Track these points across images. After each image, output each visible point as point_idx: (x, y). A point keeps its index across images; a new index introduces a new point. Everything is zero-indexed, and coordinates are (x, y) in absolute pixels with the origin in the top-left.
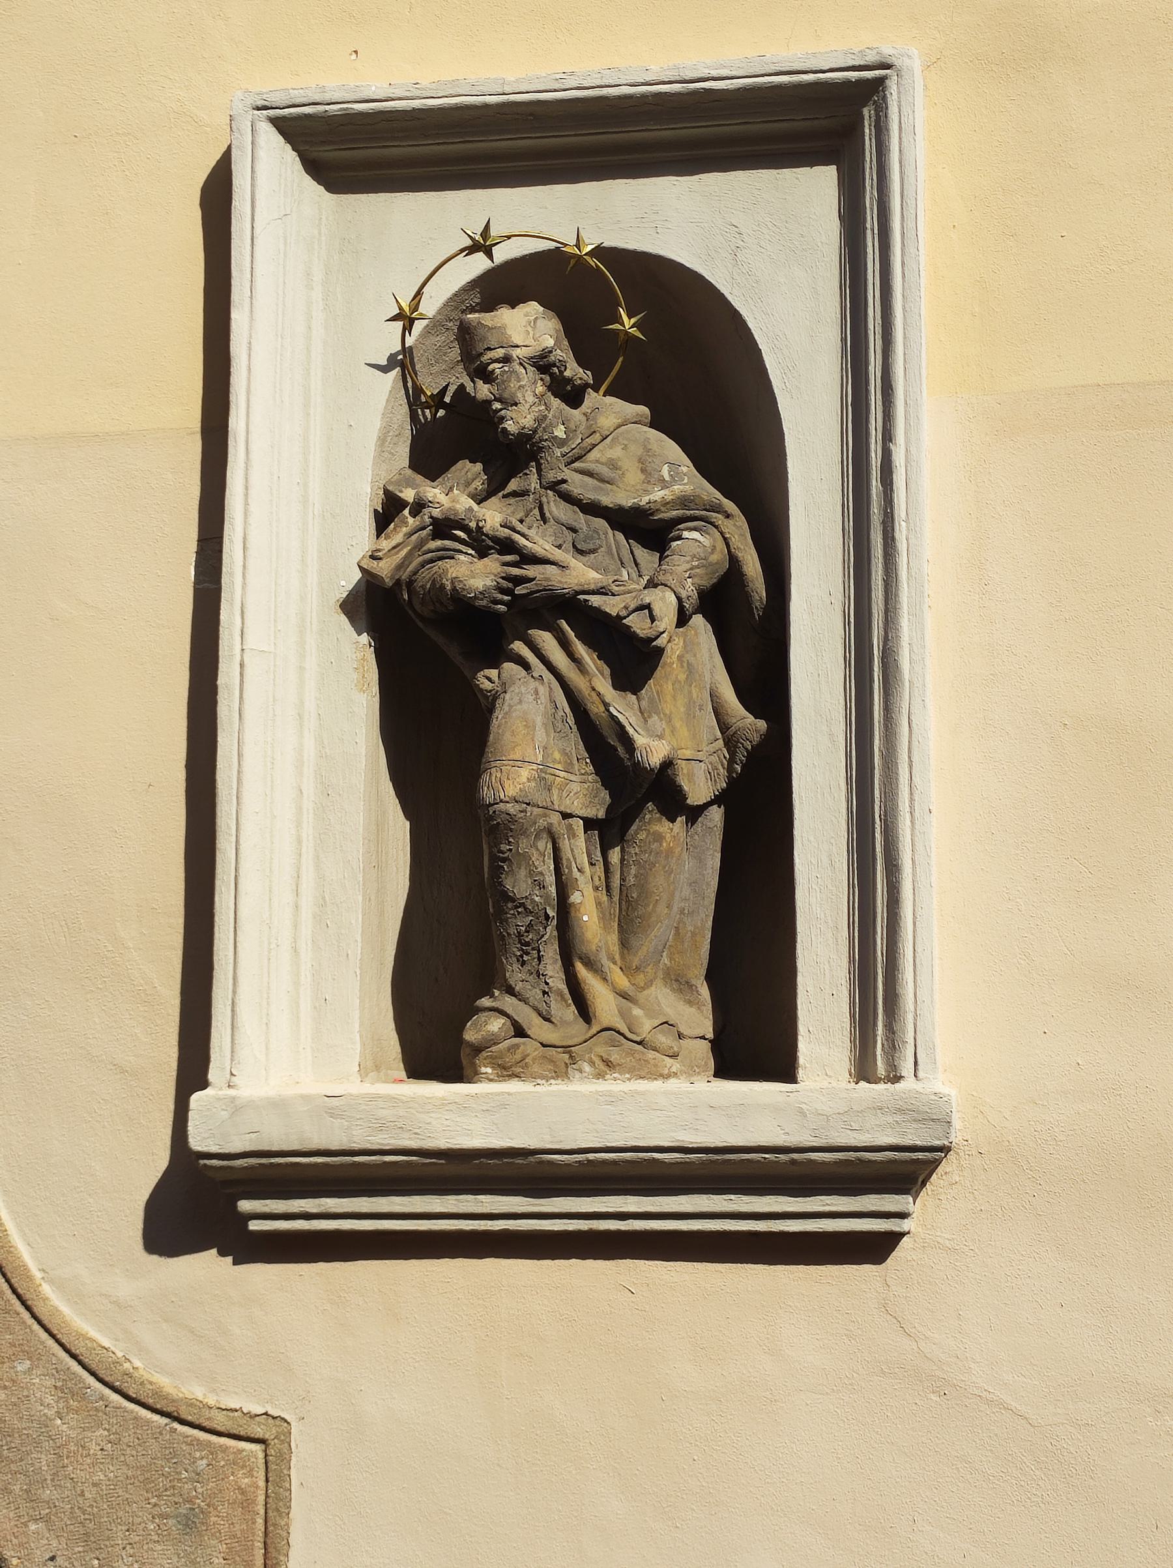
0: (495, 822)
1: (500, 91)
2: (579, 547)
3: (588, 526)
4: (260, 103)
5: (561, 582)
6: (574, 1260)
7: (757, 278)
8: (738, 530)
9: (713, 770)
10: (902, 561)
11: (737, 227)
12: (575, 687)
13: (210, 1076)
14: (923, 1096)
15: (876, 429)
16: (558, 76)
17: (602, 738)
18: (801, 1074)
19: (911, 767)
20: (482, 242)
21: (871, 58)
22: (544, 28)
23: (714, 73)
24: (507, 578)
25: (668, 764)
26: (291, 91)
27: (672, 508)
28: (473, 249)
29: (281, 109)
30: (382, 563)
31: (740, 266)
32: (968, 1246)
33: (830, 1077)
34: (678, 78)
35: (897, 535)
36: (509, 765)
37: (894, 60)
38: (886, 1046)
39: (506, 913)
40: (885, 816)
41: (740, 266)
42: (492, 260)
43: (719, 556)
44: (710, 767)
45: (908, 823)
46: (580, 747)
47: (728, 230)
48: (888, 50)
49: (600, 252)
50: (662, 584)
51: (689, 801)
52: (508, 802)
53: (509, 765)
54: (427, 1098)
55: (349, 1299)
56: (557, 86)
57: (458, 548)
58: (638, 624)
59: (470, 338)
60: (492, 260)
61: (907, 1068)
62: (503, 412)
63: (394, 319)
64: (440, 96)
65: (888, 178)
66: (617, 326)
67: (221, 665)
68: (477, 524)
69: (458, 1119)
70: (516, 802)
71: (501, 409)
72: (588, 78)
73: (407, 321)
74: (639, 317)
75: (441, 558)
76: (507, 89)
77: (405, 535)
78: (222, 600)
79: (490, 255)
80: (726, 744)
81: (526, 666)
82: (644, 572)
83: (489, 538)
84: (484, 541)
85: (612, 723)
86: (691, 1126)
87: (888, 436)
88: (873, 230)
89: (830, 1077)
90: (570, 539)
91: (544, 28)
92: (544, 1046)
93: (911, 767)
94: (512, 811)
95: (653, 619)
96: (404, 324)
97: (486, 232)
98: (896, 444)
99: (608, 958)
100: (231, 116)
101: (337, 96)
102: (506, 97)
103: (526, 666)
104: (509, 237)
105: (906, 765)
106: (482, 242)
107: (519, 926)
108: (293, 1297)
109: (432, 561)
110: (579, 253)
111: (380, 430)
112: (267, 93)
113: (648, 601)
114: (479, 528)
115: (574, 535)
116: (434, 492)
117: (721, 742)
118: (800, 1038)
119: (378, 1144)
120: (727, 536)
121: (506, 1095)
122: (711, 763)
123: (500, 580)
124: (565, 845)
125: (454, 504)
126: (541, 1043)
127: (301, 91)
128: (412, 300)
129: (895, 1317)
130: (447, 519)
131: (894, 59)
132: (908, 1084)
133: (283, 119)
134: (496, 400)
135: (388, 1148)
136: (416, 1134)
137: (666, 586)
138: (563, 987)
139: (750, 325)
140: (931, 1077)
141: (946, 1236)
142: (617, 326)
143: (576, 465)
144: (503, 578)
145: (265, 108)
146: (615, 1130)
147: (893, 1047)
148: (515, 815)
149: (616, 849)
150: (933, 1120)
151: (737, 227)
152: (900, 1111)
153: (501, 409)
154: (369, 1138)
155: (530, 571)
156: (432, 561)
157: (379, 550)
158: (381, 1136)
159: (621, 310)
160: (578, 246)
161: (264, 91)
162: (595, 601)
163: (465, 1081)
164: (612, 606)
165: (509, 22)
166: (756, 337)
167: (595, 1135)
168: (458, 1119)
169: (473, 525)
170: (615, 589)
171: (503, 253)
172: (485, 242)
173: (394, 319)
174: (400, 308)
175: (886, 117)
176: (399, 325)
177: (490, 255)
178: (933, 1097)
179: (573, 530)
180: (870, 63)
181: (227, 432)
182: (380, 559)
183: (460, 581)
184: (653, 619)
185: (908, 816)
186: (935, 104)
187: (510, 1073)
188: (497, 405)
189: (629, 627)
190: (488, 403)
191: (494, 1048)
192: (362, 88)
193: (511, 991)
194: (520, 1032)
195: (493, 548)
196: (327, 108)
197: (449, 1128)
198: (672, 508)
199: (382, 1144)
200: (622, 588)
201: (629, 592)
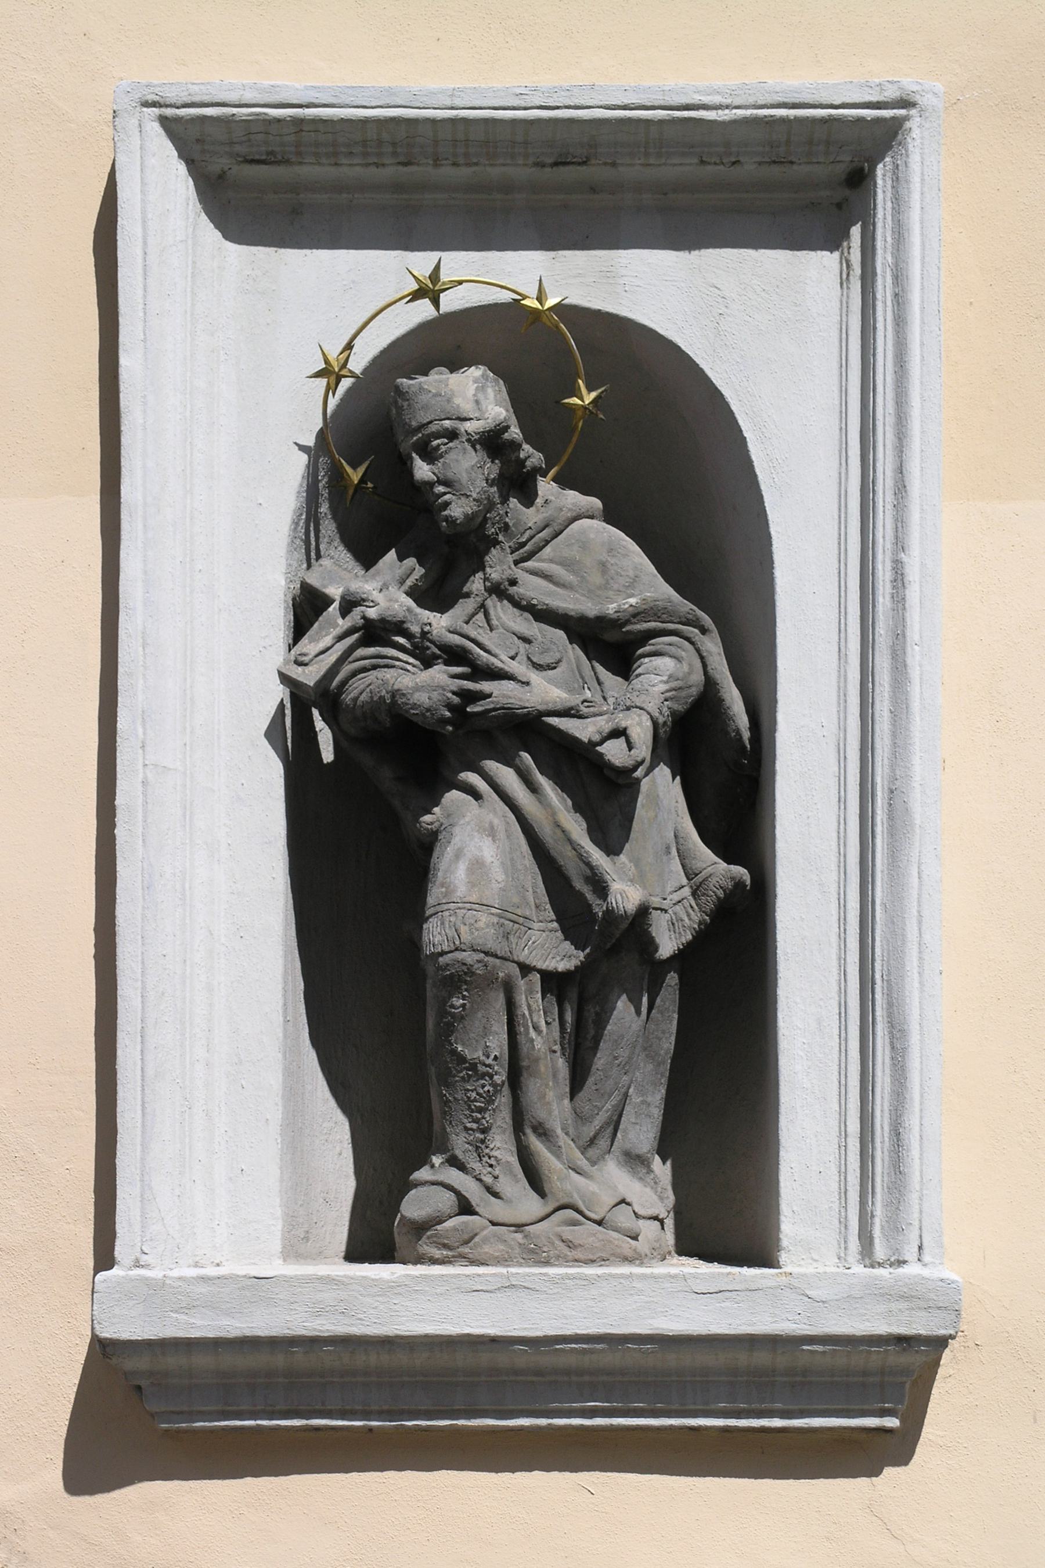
0: (448, 973)
1: (448, 103)
2: (535, 660)
3: (544, 636)
4: (151, 98)
5: (520, 700)
6: (249, 1478)
7: (742, 353)
8: (713, 646)
9: (677, 921)
10: (915, 690)
11: (719, 289)
12: (536, 822)
13: (116, 1253)
14: (929, 1282)
15: (884, 537)
16: (519, 91)
17: (567, 880)
18: (783, 1257)
19: (920, 922)
20: (431, 286)
21: (891, 93)
22: (490, 28)
23: (706, 99)
24: (461, 693)
25: (643, 911)
26: (190, 86)
27: (644, 619)
28: (416, 295)
29: (178, 108)
30: (307, 669)
31: (723, 337)
32: (962, 1443)
33: (816, 1261)
34: (662, 103)
35: (909, 661)
36: (464, 908)
37: (917, 98)
38: (886, 1228)
39: (455, 1076)
40: (889, 974)
41: (723, 337)
42: (438, 311)
43: (697, 677)
44: (674, 918)
45: (916, 985)
46: (538, 890)
47: (709, 293)
48: (909, 83)
49: (560, 309)
50: (637, 707)
51: (657, 955)
52: (464, 951)
53: (464, 908)
54: (373, 1280)
55: (268, 1502)
56: (516, 102)
57: (396, 655)
58: (614, 752)
59: (409, 405)
60: (438, 311)
61: (910, 1252)
62: (447, 497)
63: (318, 375)
64: (373, 104)
65: (907, 240)
66: (575, 400)
67: (118, 782)
68: (422, 630)
69: (407, 1304)
70: (474, 950)
71: (445, 494)
72: (555, 95)
73: (333, 379)
74: (600, 391)
75: (375, 667)
76: (458, 102)
77: (334, 638)
78: (119, 705)
79: (436, 303)
80: (694, 894)
81: (476, 795)
82: (609, 694)
83: (436, 646)
84: (428, 648)
85: (582, 866)
86: (672, 1312)
87: (900, 544)
88: (885, 303)
89: (816, 1261)
90: (522, 651)
91: (490, 28)
92: (494, 1224)
93: (920, 922)
94: (469, 961)
95: (630, 746)
96: (328, 383)
97: (435, 275)
98: (909, 555)
99: (562, 1129)
100: (114, 112)
101: (249, 96)
102: (454, 113)
103: (476, 795)
104: (460, 283)
105: (914, 921)
106: (431, 286)
107: (468, 1090)
108: (203, 1500)
109: (365, 670)
110: (540, 308)
111: (294, 511)
112: (160, 86)
113: (624, 726)
114: (424, 634)
115: (527, 646)
116: (367, 585)
117: (686, 891)
118: (782, 1218)
119: (315, 1329)
120: (705, 654)
121: (464, 1278)
122: (675, 914)
123: (450, 695)
124: (521, 999)
125: (392, 603)
126: (490, 1222)
127: (202, 87)
128: (341, 353)
129: (880, 1519)
130: (383, 620)
131: (918, 97)
132: (912, 1269)
133: (178, 120)
134: (440, 482)
135: (326, 1334)
136: (360, 1319)
137: (642, 709)
138: (514, 1160)
139: (734, 408)
140: (937, 1262)
141: (938, 1433)
142: (575, 400)
143: (529, 564)
144: (454, 693)
145: (154, 104)
146: (586, 1316)
147: (895, 1228)
148: (472, 966)
149: (619, 1004)
150: (939, 1308)
151: (719, 289)
152: (903, 1297)
153: (445, 494)
154: (305, 1324)
155: (485, 686)
156: (365, 670)
157: (305, 655)
158: (319, 1322)
159: (580, 381)
160: (540, 299)
161: (156, 82)
162: (554, 721)
163: (396, 1261)
164: (583, 730)
165: (448, 17)
166: (741, 422)
167: (565, 1321)
168: (407, 1304)
169: (415, 629)
170: (584, 710)
171: (450, 301)
172: (434, 286)
173: (318, 375)
174: (327, 361)
175: (906, 166)
176: (323, 382)
177: (436, 303)
178: (940, 1283)
179: (526, 640)
180: (889, 100)
181: (119, 503)
182: (306, 665)
183: (404, 695)
184: (630, 746)
185: (916, 976)
186: (953, 154)
187: (456, 1254)
188: (441, 489)
189: (601, 755)
190: (431, 485)
191: (438, 1227)
192: (278, 89)
193: (454, 1162)
194: (465, 1208)
195: (438, 657)
196: (235, 110)
197: (398, 1313)
198: (644, 619)
199: (320, 1331)
200: (592, 709)
201: (601, 714)
